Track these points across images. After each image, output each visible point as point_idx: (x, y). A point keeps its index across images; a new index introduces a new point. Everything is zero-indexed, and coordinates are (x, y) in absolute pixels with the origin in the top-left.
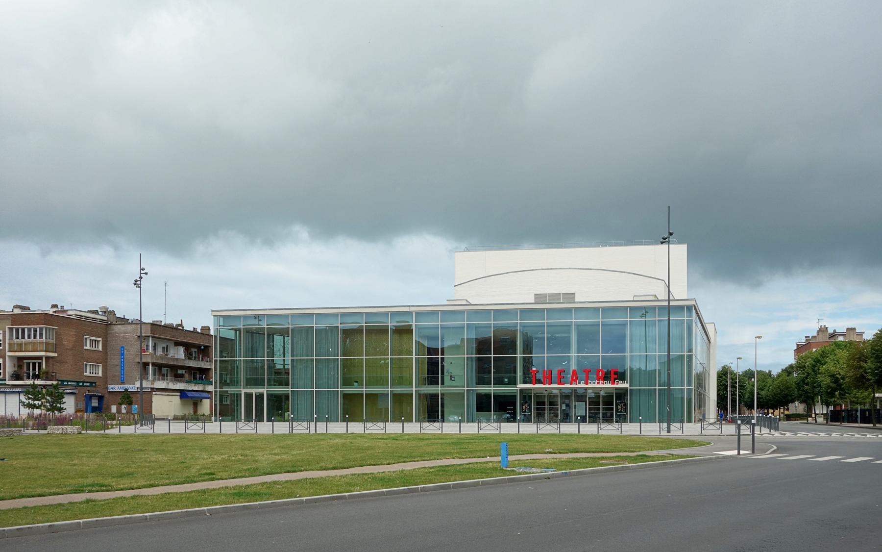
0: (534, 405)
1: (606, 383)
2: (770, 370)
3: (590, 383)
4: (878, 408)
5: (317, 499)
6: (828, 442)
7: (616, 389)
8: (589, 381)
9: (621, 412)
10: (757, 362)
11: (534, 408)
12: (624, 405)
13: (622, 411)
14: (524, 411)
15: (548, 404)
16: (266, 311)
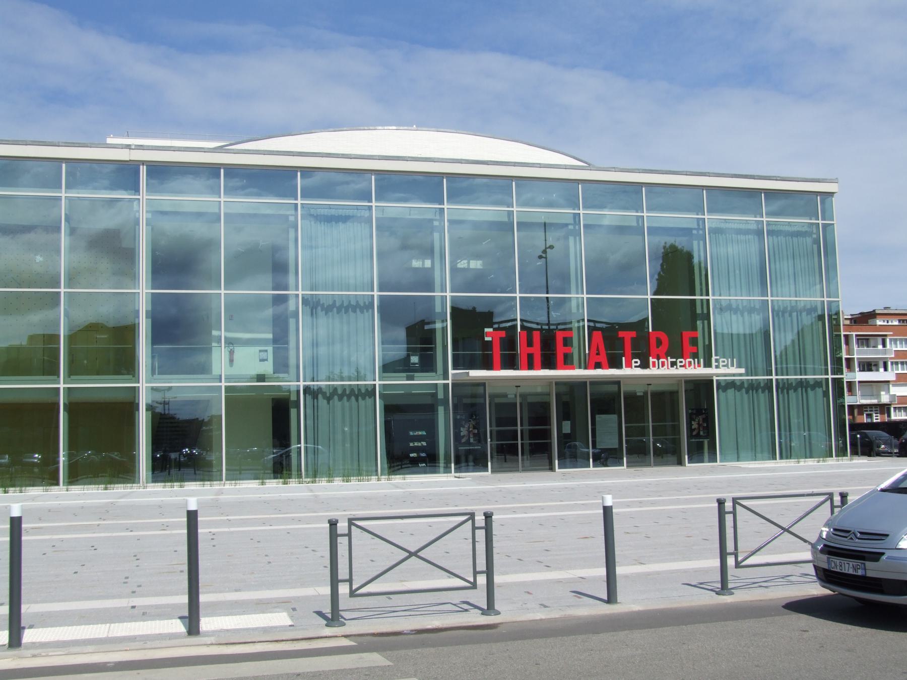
0: (491, 426)
1: (690, 363)
2: (554, 246)
3: (654, 363)
4: (706, 407)
5: (210, 521)
6: (514, 622)
7: (557, 384)
8: (651, 360)
9: (468, 443)
10: (544, 233)
11: (491, 432)
12: (704, 420)
13: (702, 433)
14: (694, 433)
15: (494, 423)
16: (295, 350)
